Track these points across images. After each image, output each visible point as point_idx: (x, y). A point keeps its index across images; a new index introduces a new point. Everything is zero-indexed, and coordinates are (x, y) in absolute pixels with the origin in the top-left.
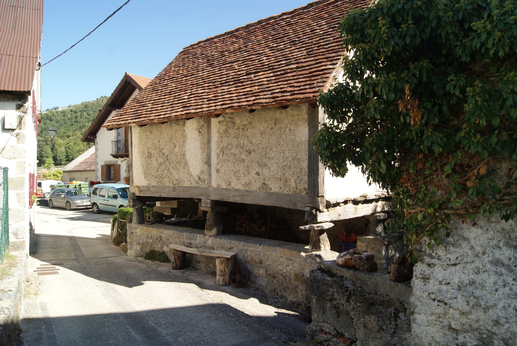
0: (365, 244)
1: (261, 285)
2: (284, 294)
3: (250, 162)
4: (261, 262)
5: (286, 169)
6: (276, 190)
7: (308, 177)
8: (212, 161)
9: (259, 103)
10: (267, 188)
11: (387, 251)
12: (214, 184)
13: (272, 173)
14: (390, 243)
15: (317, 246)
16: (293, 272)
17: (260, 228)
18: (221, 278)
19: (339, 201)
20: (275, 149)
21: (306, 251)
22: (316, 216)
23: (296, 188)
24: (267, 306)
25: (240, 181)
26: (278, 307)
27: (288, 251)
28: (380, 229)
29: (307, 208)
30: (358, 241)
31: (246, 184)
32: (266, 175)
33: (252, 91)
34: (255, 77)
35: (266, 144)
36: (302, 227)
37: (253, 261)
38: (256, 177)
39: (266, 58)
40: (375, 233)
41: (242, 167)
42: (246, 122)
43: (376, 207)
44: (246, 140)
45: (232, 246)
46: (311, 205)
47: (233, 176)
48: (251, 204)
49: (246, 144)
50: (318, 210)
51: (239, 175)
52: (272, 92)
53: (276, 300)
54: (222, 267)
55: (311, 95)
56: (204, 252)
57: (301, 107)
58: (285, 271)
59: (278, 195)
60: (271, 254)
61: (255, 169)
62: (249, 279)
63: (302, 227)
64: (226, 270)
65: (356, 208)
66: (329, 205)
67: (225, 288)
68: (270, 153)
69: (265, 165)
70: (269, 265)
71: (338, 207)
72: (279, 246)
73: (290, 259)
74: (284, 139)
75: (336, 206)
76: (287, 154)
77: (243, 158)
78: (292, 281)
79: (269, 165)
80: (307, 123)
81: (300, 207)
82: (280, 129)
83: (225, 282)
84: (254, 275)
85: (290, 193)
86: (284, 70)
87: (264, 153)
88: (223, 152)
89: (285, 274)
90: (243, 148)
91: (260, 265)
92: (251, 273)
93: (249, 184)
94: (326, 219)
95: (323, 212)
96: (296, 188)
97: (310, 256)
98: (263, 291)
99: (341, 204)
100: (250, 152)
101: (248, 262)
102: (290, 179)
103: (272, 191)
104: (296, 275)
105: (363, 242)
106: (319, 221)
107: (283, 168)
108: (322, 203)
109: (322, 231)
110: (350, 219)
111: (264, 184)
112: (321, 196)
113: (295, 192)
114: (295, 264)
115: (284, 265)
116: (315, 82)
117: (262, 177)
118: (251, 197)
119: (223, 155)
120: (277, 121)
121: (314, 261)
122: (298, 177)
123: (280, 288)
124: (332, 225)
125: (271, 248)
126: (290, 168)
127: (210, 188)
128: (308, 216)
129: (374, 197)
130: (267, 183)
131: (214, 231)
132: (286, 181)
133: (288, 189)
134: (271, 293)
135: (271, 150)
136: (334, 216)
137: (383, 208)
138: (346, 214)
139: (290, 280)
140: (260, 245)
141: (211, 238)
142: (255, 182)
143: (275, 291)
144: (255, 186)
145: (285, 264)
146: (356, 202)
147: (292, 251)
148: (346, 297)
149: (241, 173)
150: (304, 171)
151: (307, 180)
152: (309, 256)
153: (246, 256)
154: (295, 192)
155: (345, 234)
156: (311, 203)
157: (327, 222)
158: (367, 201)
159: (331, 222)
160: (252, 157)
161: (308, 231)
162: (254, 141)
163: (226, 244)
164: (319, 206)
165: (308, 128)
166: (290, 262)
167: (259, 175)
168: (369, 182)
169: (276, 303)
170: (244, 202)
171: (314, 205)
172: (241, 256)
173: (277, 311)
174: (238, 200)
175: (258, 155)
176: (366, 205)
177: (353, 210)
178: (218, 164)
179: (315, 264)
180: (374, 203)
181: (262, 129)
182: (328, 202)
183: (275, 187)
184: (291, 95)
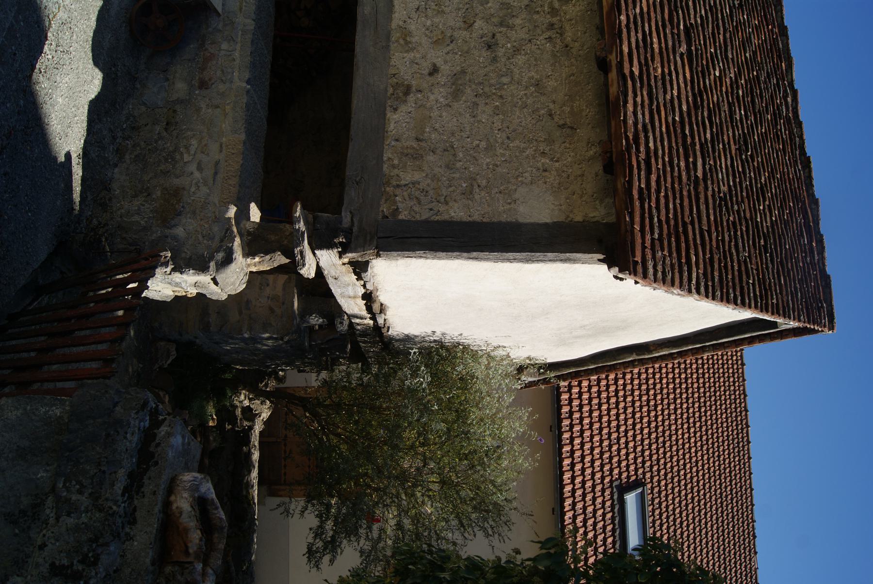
2: (127, 157)
3: (465, 48)
4: (203, 85)
6: (392, 126)
7: (427, 222)
9: (626, 95)
10: (397, 99)
20: (498, 125)
23: (398, 186)
25: (414, 15)
29: (349, 219)
30: (286, 277)
31: (406, 34)
32: (432, 97)
33: (653, 60)
34: (682, 55)
35: (512, 96)
38: (426, 67)
39: (717, 74)
41: (452, 23)
42: (569, 36)
44: (523, 34)
46: (355, 229)
48: (353, 50)
49: (512, 34)
52: (649, 127)
55: (638, 258)
57: (601, 201)
58: (186, 158)
59: (379, 130)
60: (226, 115)
61: (446, 62)
69: (456, 94)
70: (198, 110)
73: (216, 173)
74: (523, 151)
79: (456, 105)
80: (562, 218)
81: (351, 194)
82: (550, 141)
86: (693, 144)
87: (487, 89)
89: (178, 157)
90: (501, 24)
91: (196, 83)
93: (407, 43)
96: (398, 186)
102: (420, 168)
103: (389, 115)
105: (284, 289)
107: (449, 149)
111: (408, 90)
113: (388, 183)
114: (204, 190)
116: (666, 253)
117: (425, 85)
120: (568, 131)
122: (425, 192)
130: (411, 98)
132: (417, 156)
133: (396, 162)
135: (496, 111)
139: (165, 173)
140: (248, 82)
142: (413, 62)
143: (133, 128)
144: (401, 63)
148: (65, 562)
149: (436, 20)
150: (442, 208)
151: (418, 217)
152: (229, 229)
154: (388, 183)
160: (476, 53)
161: (291, 221)
162: (520, 59)
165: (548, 221)
167: (431, 74)
170: (359, 28)
173: (74, 156)
181: (552, 83)
183: (399, 121)
184: (640, 190)
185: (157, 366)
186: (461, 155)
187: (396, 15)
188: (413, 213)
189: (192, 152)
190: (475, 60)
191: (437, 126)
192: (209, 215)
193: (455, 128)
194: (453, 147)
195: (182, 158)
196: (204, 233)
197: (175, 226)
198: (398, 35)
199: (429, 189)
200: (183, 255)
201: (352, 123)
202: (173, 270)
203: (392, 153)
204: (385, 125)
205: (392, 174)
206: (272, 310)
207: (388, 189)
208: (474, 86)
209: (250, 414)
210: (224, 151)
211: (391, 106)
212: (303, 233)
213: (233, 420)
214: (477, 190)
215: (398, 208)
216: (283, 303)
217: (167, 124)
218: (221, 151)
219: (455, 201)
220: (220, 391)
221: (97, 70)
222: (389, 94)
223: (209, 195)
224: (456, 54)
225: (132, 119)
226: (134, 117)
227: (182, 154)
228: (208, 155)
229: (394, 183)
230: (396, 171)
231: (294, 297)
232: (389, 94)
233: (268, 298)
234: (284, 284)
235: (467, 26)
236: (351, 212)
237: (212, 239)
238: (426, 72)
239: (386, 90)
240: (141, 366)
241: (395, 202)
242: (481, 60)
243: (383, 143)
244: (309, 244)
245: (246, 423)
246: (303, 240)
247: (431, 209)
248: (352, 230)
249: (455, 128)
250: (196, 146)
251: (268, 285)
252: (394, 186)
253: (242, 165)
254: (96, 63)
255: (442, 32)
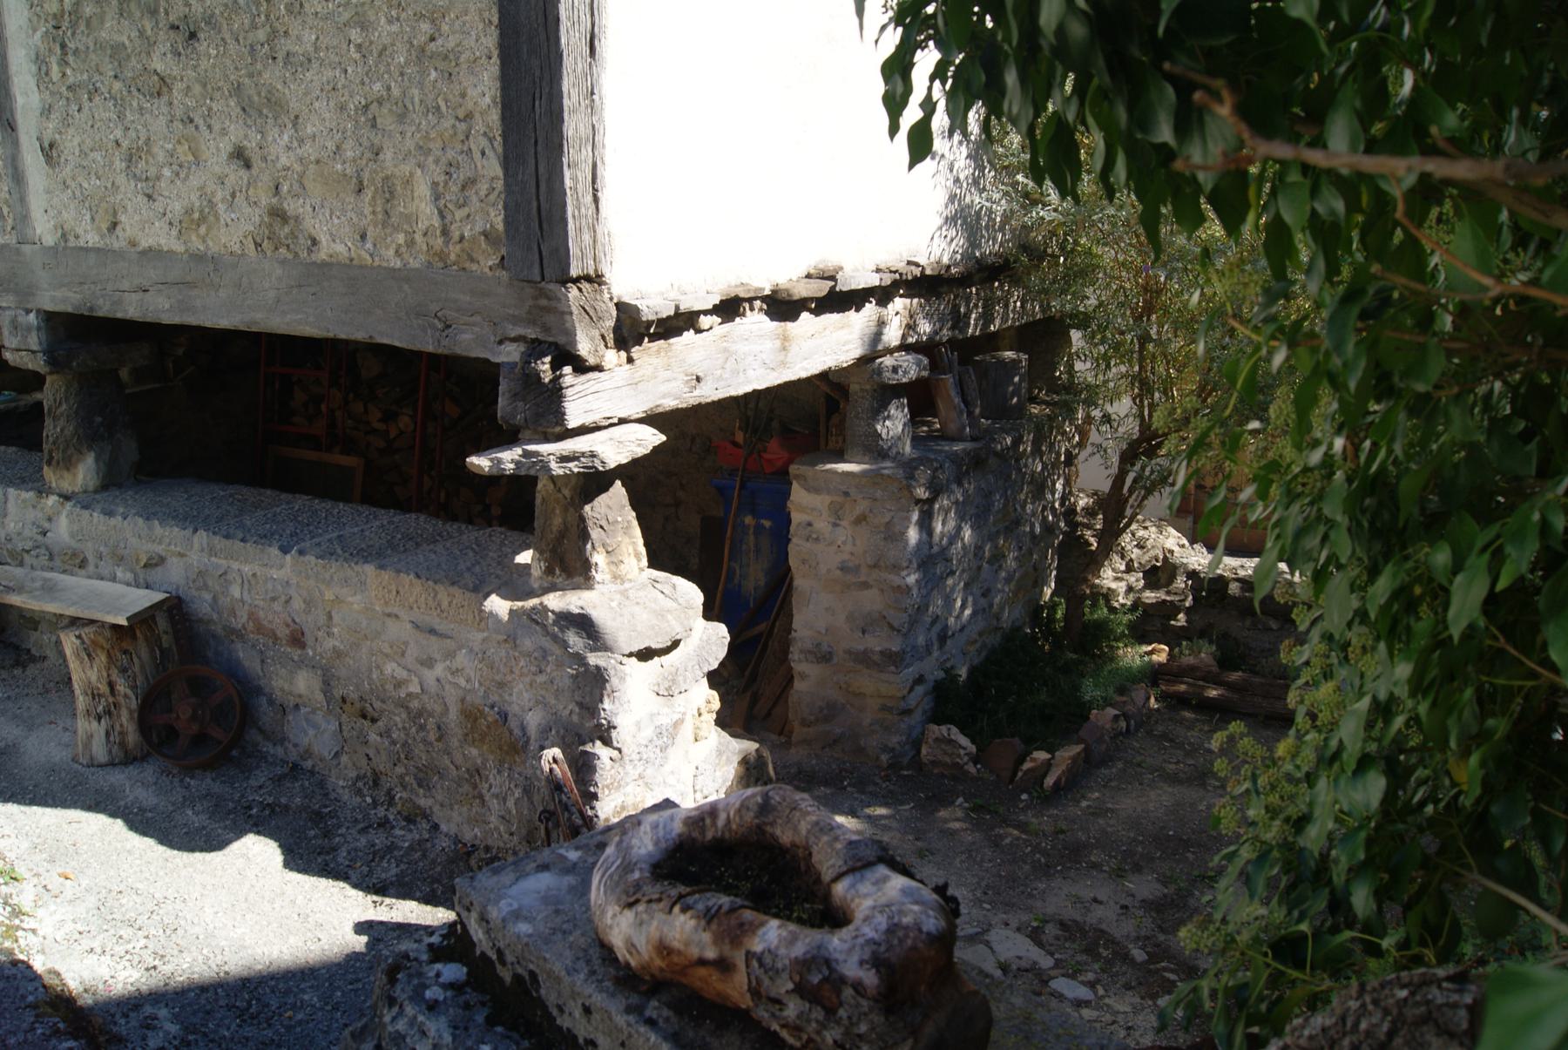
0: (827, 499)
1: (307, 754)
2: (422, 802)
3: (197, 89)
4: (298, 640)
5: (386, 121)
7: (506, 163)
8: (20, 101)
10: (293, 235)
11: (925, 524)
12: (43, 228)
13: (309, 150)
14: (936, 490)
15: (570, 564)
16: (452, 696)
17: (389, 417)
18: (98, 729)
19: (690, 304)
21: (515, 585)
22: (555, 394)
23: (445, 232)
24: (323, 883)
25: (159, 206)
26: (379, 889)
27: (418, 587)
28: (894, 424)
30: (795, 485)
32: (284, 161)
36: (481, 462)
37: (260, 629)
40: (875, 449)
41: (162, 120)
43: (881, 323)
45: (160, 549)
46: (531, 333)
47: (121, 179)
50: (567, 357)
51: (152, 171)
53: (380, 840)
54: (93, 675)
56: (19, 589)
58: (414, 688)
59: (349, 274)
61: (224, 132)
62: (247, 716)
63: (481, 462)
64: (121, 687)
65: (785, 339)
66: (631, 331)
67: (117, 777)
68: (295, 27)
70: (338, 654)
71: (689, 335)
72: (375, 555)
73: (432, 631)
75: (678, 332)
76: (384, 30)
77: (159, 67)
78: (455, 742)
81: (469, 342)
83: (122, 744)
84: (271, 702)
85: (414, 264)
87: (261, 35)
88: (63, 46)
89: (415, 704)
91: (296, 654)
92: (259, 691)
93: (203, 219)
94: (613, 409)
95: (598, 368)
96: (445, 232)
97: (536, 618)
98: (322, 784)
99: (705, 321)
100: (193, 36)
101: (239, 634)
102: (408, 182)
103: (322, 255)
104: (471, 715)
105: (816, 490)
106: (572, 423)
108: (591, 316)
109: (594, 482)
110: (756, 394)
112: (588, 279)
113: (442, 256)
114: (462, 659)
115: (409, 659)
118: (222, 293)
119: (63, 62)
121: (557, 650)
123: (400, 770)
124: (650, 438)
125: (335, 569)
126: (402, 117)
127: (26, 248)
128: (515, 396)
129: (874, 280)
130: (292, 206)
131: (84, 473)
132: (388, 192)
133: (401, 238)
134: (359, 792)
136: (664, 388)
137: (911, 327)
138: (736, 372)
140: (285, 550)
141: (69, 505)
144: (234, 231)
145: (412, 652)
146: (782, 307)
147: (439, 587)
150: (479, 127)
151: (499, 185)
153: (224, 601)
154: (442, 256)
155: (740, 437)
156: (532, 322)
157: (622, 421)
158: (839, 300)
159: (653, 419)
160: (204, 64)
163: (134, 541)
164: (571, 334)
166: (434, 646)
167: (248, 166)
168: (911, 115)
169: (376, 855)
171: (546, 329)
172: (202, 605)
174: (161, 308)
175: (232, 45)
176: (835, 316)
177: (769, 346)
178: (47, 111)
179: (560, 665)
180: (870, 309)
182: (625, 311)
183: (332, 233)
185: (971, 769)
186: (377, 87)
187: (163, 242)
188: (492, 197)
189: (405, 674)
190: (214, 66)
191: (331, 145)
192: (503, 654)
193: (332, 104)
194: (366, 107)
195: (417, 696)
196: (533, 669)
197: (523, 728)
198: (194, 238)
199: (444, 160)
200: (575, 718)
201: (343, 336)
202: (607, 742)
203: (387, 248)
204: (339, 264)
205: (425, 248)
206: (860, 520)
207: (453, 257)
208: (259, 66)
209: (1160, 573)
210: (395, 610)
211: (310, 251)
212: (526, 454)
213: (1166, 610)
214: (440, 42)
215: (485, 234)
216: (846, 494)
217: (364, 717)
218: (397, 616)
219: (463, 95)
220: (1087, 636)
221: (236, 846)
222: (290, 256)
223: (471, 650)
224: (210, 109)
225: (360, 784)
226: (358, 778)
227: (409, 695)
228: (406, 643)
229: (440, 241)
230: (418, 237)
231: (835, 472)
232: (290, 256)
233: (835, 525)
234: (808, 490)
235: (165, 89)
236: (501, 342)
237: (545, 653)
238: (243, 172)
239: (283, 262)
240: (961, 800)
241: (474, 239)
242: (213, 52)
243: (372, 268)
244: (547, 439)
245: (1180, 582)
246: (536, 454)
247: (483, 154)
248: (534, 341)
249: (332, 104)
250: (394, 665)
251: (810, 524)
252: (447, 243)
253: (418, 576)
254: (214, 843)
255: (179, 142)
